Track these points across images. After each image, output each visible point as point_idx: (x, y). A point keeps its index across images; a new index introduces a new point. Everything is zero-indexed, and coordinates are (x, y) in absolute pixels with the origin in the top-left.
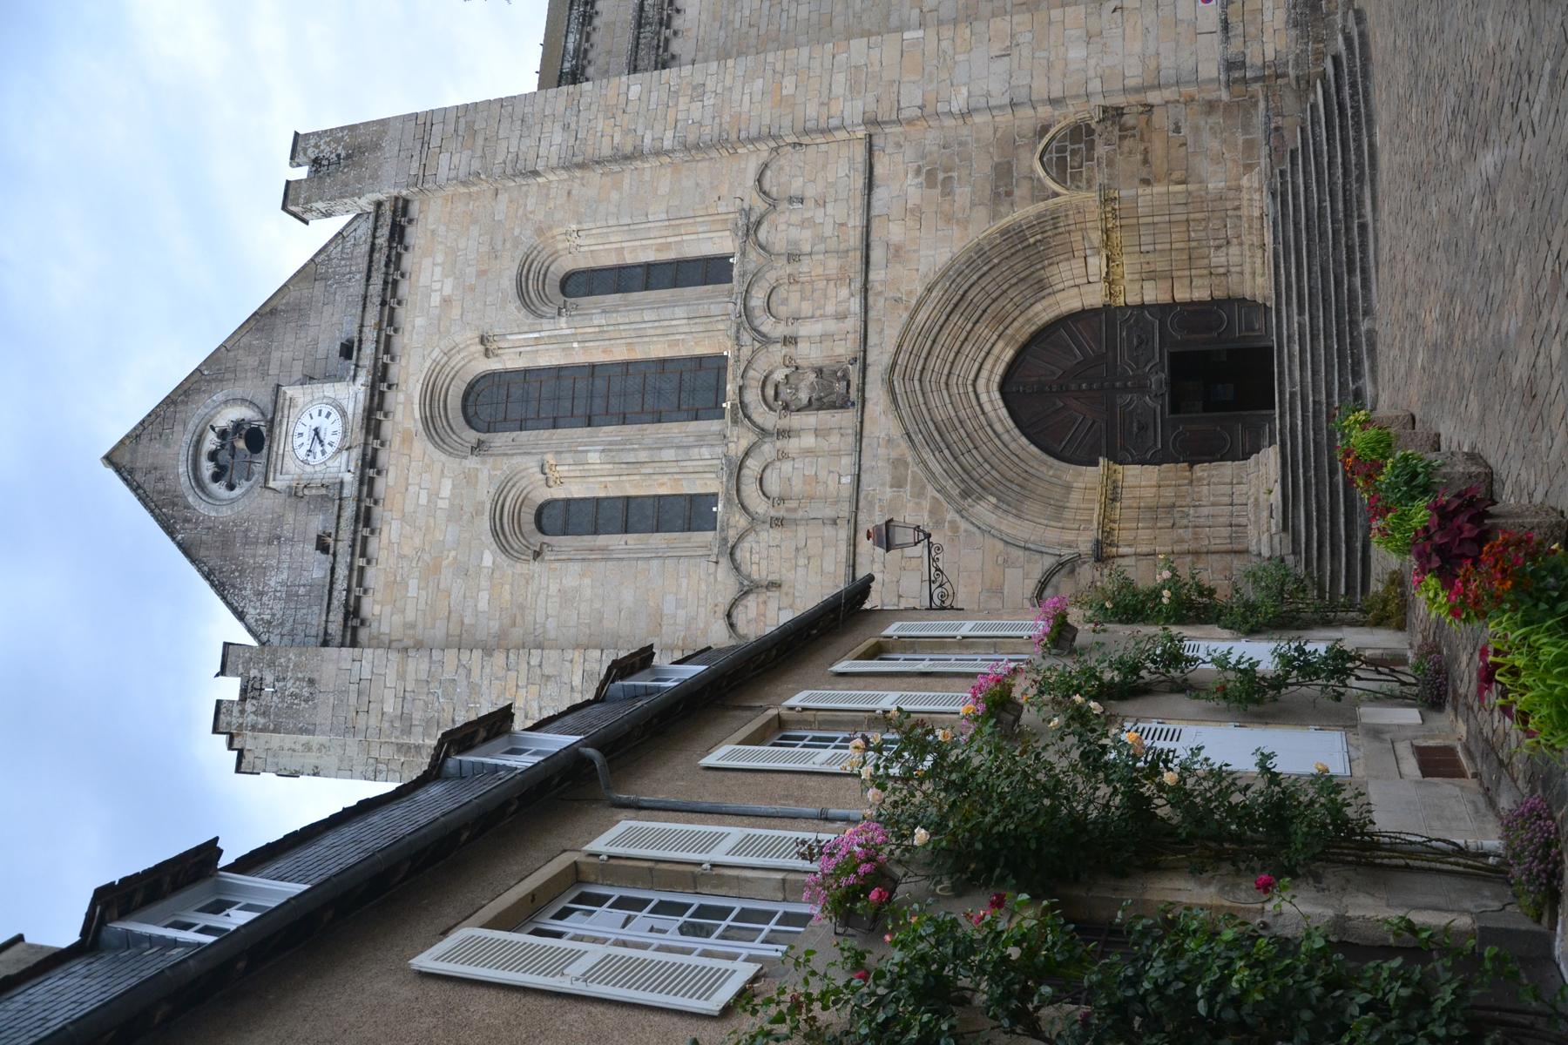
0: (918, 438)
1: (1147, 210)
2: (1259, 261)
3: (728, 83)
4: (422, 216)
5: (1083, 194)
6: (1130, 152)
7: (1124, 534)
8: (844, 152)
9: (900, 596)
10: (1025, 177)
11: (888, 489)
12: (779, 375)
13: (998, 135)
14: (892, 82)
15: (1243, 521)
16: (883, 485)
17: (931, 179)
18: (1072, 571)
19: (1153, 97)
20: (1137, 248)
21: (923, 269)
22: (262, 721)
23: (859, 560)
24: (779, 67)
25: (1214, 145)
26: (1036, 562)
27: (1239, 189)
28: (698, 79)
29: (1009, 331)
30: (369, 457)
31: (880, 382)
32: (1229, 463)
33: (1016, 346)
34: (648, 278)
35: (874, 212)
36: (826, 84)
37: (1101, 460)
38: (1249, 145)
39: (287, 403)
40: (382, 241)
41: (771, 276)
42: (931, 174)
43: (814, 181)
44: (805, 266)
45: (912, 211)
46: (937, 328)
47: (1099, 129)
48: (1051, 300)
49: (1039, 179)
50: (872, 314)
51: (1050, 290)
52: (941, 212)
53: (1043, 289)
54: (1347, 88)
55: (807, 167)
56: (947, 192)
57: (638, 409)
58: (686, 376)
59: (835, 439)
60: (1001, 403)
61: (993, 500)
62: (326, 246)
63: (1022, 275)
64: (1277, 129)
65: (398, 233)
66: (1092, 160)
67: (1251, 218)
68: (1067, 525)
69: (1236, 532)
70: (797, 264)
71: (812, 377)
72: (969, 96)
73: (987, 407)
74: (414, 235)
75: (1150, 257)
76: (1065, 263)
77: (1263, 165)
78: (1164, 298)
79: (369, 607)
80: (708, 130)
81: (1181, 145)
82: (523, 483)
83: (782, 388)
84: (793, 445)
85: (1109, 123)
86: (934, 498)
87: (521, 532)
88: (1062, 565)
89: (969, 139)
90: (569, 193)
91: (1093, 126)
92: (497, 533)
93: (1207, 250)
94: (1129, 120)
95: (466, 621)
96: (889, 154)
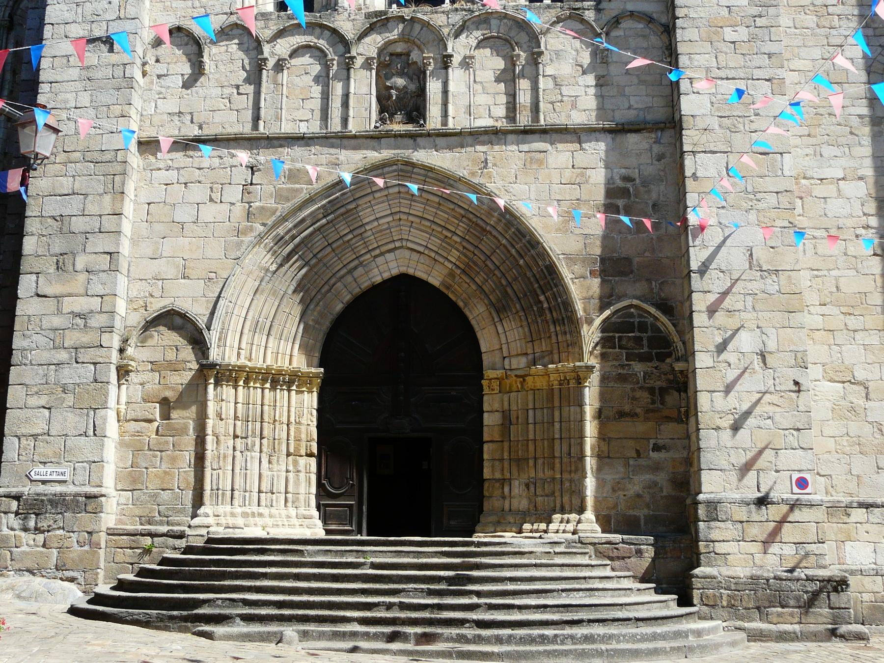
6: (634, 398)
9: (186, 184)
37: (322, 370)
51: (496, 320)
54: (374, 630)
86: (277, 209)
96: (651, 148)
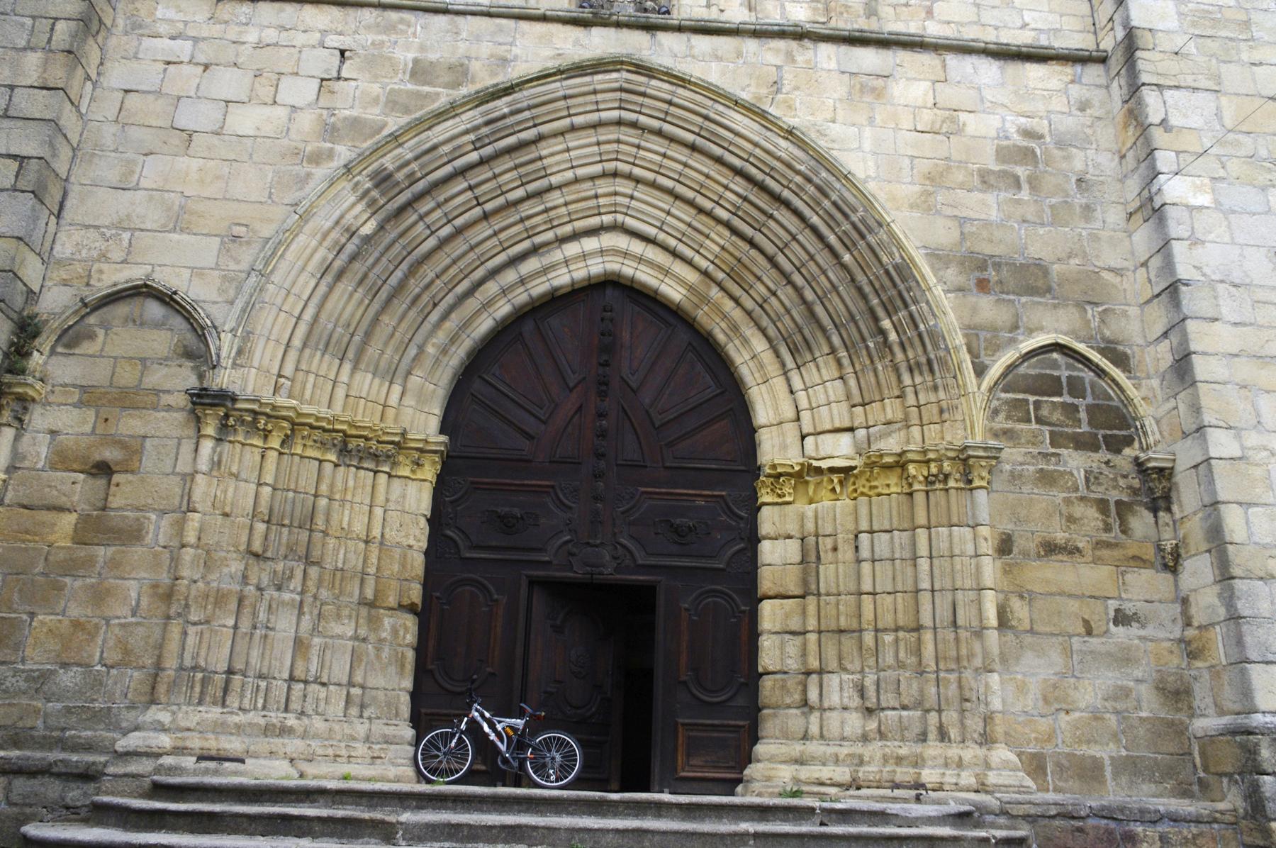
0: (502, 105)
1: (943, 546)
2: (825, 773)
5: (980, 419)
6: (1071, 519)
7: (252, 457)
9: (206, 67)
11: (411, 56)
13: (1104, 274)
14: (1218, 78)
15: (233, 701)
16: (422, 48)
18: (189, 354)
19: (1198, 570)
20: (864, 525)
21: (835, 130)
26: (221, 291)
27: (987, 740)
29: (715, 292)
32: (408, 683)
33: (687, 306)
35: (952, 60)
38: (1090, 772)
42: (1027, 155)
45: (953, 121)
46: (718, 151)
48: (772, 367)
49: (1013, 341)
50: (751, 45)
51: (790, 363)
52: (949, 167)
53: (794, 351)
56: (986, 180)
61: (368, 229)
63: (819, 310)
67: (918, 762)
68: (292, 356)
69: (205, 682)
72: (1191, 209)
73: (572, 249)
75: (846, 553)
77: (1039, 797)
78: (766, 581)
81: (1086, 623)
85: (1136, 483)
88: (202, 338)
89: (1098, 224)
91: (1127, 451)
93: (857, 666)
96: (1066, 92)
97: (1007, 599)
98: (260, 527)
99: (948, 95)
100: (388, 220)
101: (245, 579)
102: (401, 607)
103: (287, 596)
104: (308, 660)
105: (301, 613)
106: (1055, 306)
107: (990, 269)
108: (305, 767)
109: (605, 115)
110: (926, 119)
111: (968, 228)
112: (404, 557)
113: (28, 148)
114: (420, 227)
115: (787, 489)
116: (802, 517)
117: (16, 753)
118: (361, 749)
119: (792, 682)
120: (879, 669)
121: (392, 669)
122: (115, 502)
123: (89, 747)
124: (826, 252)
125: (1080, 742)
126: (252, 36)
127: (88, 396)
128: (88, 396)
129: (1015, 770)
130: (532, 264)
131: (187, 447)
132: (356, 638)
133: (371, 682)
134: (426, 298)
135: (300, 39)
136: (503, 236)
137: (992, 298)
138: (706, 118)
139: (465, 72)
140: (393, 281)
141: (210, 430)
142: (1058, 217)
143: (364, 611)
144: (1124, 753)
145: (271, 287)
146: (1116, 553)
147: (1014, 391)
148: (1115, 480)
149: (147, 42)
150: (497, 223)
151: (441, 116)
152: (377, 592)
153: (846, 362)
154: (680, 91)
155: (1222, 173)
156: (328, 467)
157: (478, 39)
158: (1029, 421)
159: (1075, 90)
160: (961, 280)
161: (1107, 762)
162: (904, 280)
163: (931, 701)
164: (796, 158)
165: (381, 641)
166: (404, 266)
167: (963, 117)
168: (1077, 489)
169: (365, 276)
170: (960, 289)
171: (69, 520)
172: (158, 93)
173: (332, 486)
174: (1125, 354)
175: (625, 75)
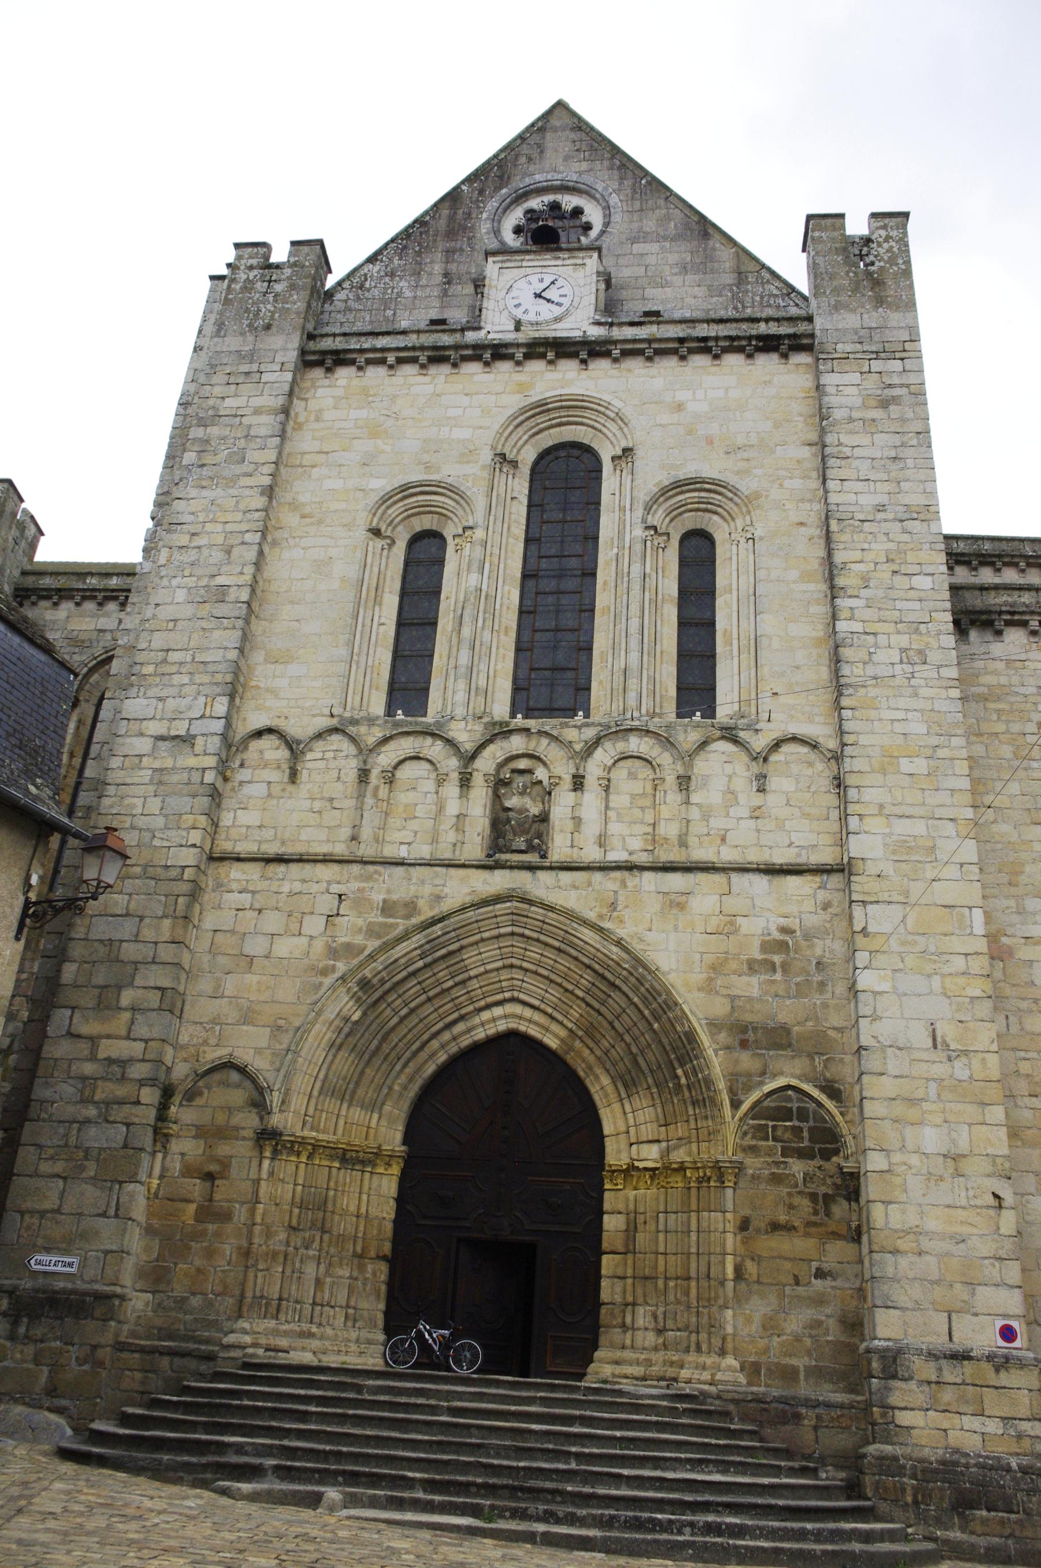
0: (437, 930)
1: (705, 1224)
2: (629, 1370)
3: (924, 692)
4: (793, 367)
6: (791, 1207)
8: (827, 839)
9: (260, 911)
10: (765, 1066)
11: (382, 897)
12: (541, 773)
15: (282, 1317)
16: (389, 892)
17: (771, 946)
21: (650, 937)
22: (237, 287)
23: (308, 867)
24: (941, 753)
25: (795, 1323)
26: (272, 1063)
27: (722, 1353)
28: (933, 657)
30: (504, 351)
31: (511, 886)
32: (382, 1306)
33: (560, 1052)
34: (696, 625)
35: (735, 877)
36: (909, 811)
38: (789, 1374)
39: (579, 261)
40: (762, 328)
41: (665, 758)
42: (782, 946)
43: (788, 804)
44: (674, 797)
45: (732, 923)
47: (829, 1166)
48: (613, 1096)
49: (762, 1083)
50: (598, 876)
51: (624, 1095)
52: (727, 959)
55: (808, 795)
56: (752, 966)
57: (538, 625)
58: (570, 674)
59: (451, 837)
60: (491, 1032)
62: (777, 277)
63: (640, 1059)
64: (797, 1417)
65: (769, 344)
66: (783, 1156)
68: (313, 1101)
69: (267, 1305)
70: (676, 788)
71: (535, 810)
72: (875, 993)
73: (486, 1015)
74: (767, 363)
76: (653, 1116)
79: (344, 375)
80: (858, 670)
82: (460, 512)
83: (526, 778)
84: (452, 790)
85: (839, 1181)
86: (365, 947)
87: (409, 517)
88: (262, 1094)
89: (829, 995)
90: (802, 524)
91: (834, 1159)
92: (405, 490)
94: (840, 1209)
95: (315, 470)
96: (814, 896)
97: (743, 1261)
98: (296, 1211)
99: (732, 904)
100: (368, 1008)
101: (288, 1244)
102: (378, 1257)
103: (311, 1253)
104: (323, 1291)
105: (319, 1263)
106: (793, 1057)
107: (750, 1032)
108: (321, 1356)
109: (502, 931)
110: (714, 923)
111: (737, 1003)
112: (380, 1225)
113: (165, 983)
114: (389, 1010)
115: (619, 1181)
116: (627, 1199)
117: (171, 1344)
118: (353, 1347)
119: (617, 1311)
120: (667, 1304)
121: (372, 1298)
122: (217, 1197)
123: (207, 1341)
124: (643, 1022)
125: (785, 1355)
126: (286, 888)
127: (201, 1132)
128: (201, 1132)
129: (735, 1371)
130: (460, 1027)
131: (255, 1163)
132: (351, 1277)
133: (360, 1305)
134: (393, 1055)
135: (315, 888)
136: (441, 1011)
137: (750, 1053)
138: (566, 932)
139: (415, 907)
140: (373, 1047)
141: (268, 1154)
142: (801, 991)
143: (356, 1261)
144: (814, 1363)
145: (300, 1060)
146: (820, 1230)
147: (759, 1119)
148: (824, 1179)
149: (227, 896)
150: (437, 1003)
151: (399, 940)
152: (363, 1249)
153: (656, 1096)
154: (550, 914)
155: (901, 966)
156: (334, 1171)
157: (423, 882)
158: (767, 1139)
159: (822, 895)
160: (729, 1041)
161: (802, 1369)
162: (690, 1043)
163: (693, 1327)
164: (622, 959)
165: (366, 1279)
166: (379, 1037)
167: (739, 920)
168: (797, 1186)
169: (355, 1046)
170: (728, 1048)
171: (192, 1208)
172: (233, 932)
173: (336, 1182)
174: (839, 1090)
175: (515, 904)
